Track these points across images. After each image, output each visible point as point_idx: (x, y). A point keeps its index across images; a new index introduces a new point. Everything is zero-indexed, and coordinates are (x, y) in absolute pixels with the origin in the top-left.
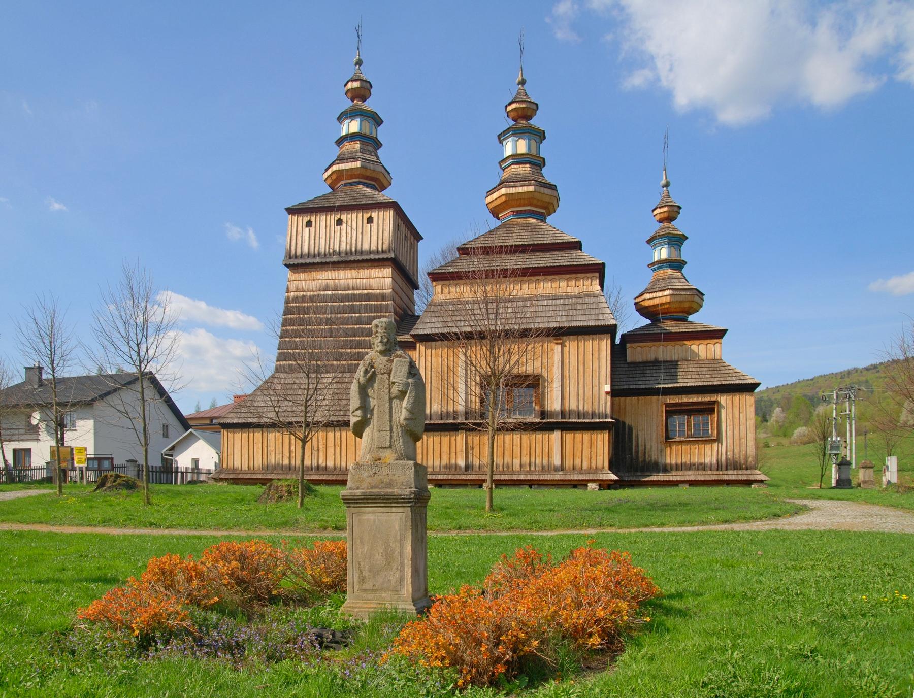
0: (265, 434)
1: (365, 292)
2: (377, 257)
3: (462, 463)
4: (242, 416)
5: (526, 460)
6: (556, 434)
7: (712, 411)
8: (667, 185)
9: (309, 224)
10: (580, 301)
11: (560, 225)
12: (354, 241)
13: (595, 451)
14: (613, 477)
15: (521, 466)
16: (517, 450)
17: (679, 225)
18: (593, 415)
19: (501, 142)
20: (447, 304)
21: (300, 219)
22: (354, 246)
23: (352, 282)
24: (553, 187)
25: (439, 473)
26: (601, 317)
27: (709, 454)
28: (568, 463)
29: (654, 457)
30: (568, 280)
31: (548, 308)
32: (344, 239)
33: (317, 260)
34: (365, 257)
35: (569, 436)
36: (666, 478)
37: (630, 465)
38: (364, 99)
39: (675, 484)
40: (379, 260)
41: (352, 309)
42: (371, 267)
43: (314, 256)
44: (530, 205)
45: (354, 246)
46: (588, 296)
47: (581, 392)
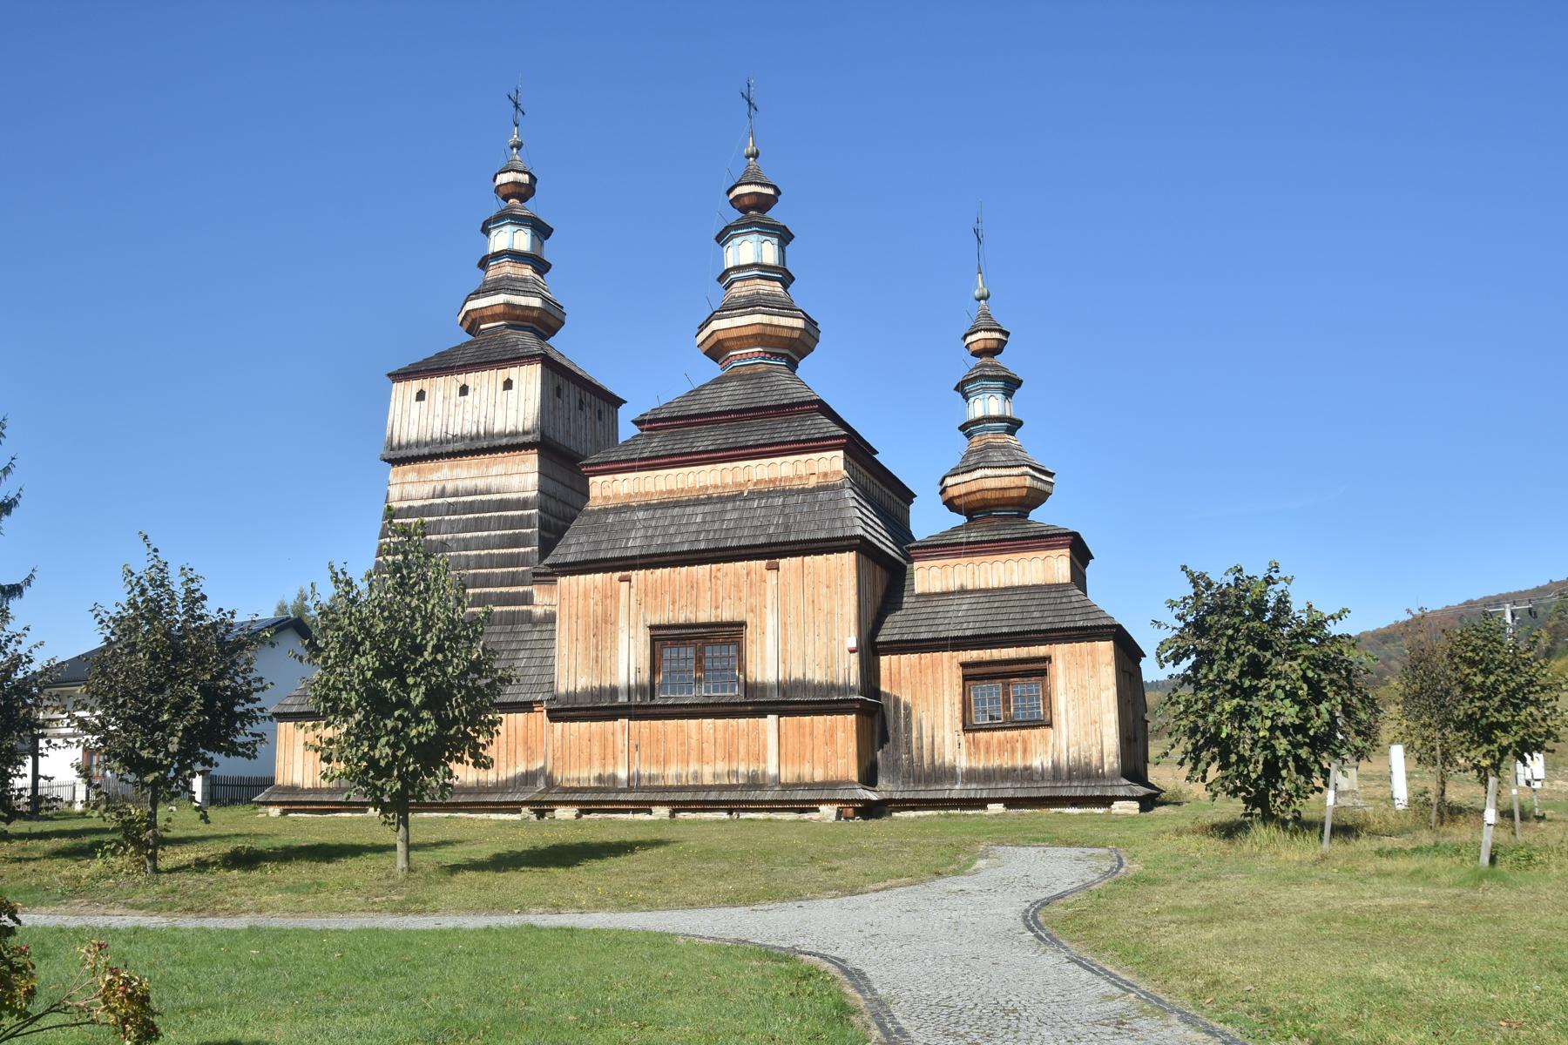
6: (772, 718)
11: (817, 376)
13: (832, 747)
29: (948, 759)
35: (789, 722)
41: (478, 525)
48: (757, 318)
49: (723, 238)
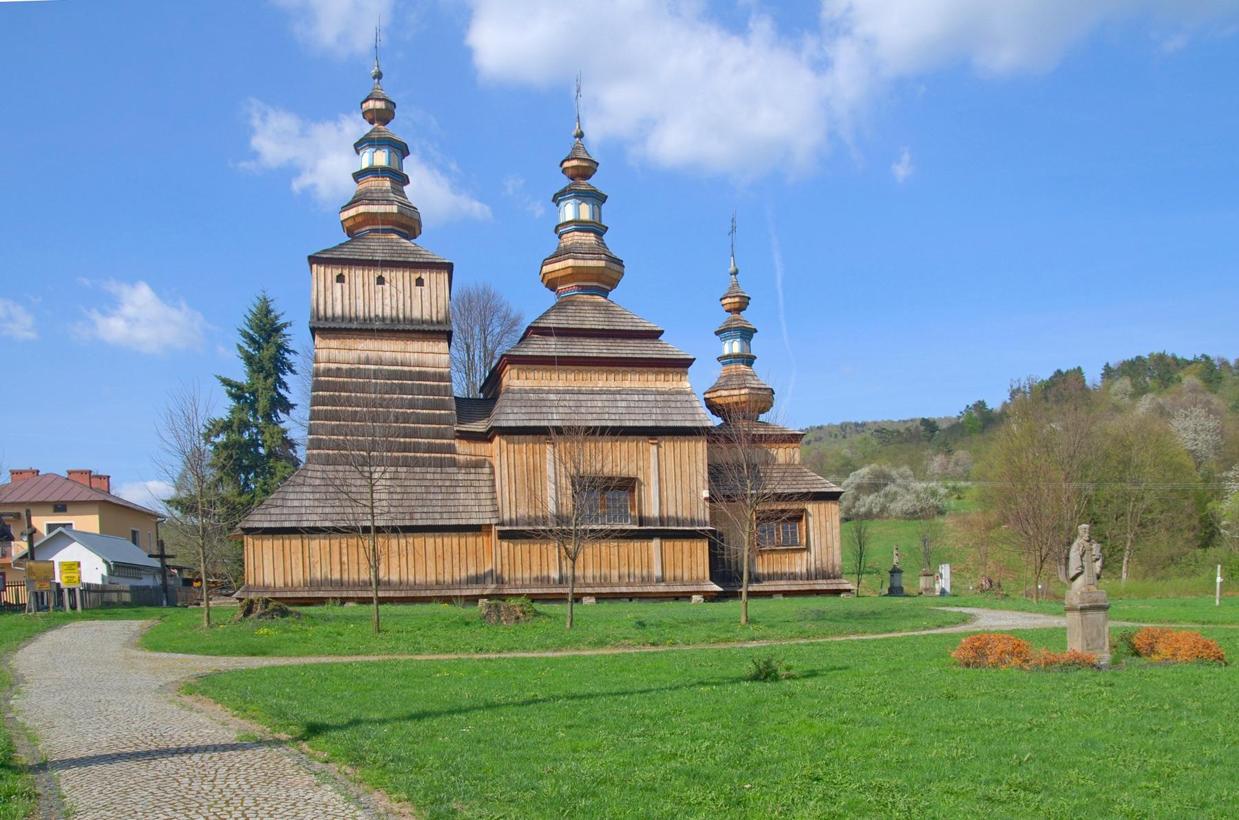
0: (306, 542)
1: (417, 369)
2: (432, 328)
3: (555, 575)
4: (274, 518)
5: (625, 570)
6: (655, 543)
7: (799, 519)
8: (736, 273)
9: (340, 279)
10: (672, 398)
12: (401, 306)
13: (693, 562)
14: (717, 588)
15: (620, 577)
16: (615, 559)
17: (749, 317)
18: (692, 522)
19: (358, 153)
20: (526, 392)
21: (329, 271)
22: (401, 311)
23: (399, 356)
24: (619, 262)
25: (530, 587)
26: (697, 417)
27: (799, 563)
28: (669, 574)
30: (657, 373)
31: (640, 404)
32: (387, 301)
33: (355, 325)
34: (417, 327)
35: (668, 544)
36: (761, 589)
37: (727, 576)
38: (385, 121)
39: (768, 594)
40: (434, 332)
41: (403, 389)
42: (423, 340)
43: (351, 320)
44: (598, 281)
45: (401, 311)
46: (679, 393)
47: (679, 497)
48: (570, 262)
49: (558, 198)
